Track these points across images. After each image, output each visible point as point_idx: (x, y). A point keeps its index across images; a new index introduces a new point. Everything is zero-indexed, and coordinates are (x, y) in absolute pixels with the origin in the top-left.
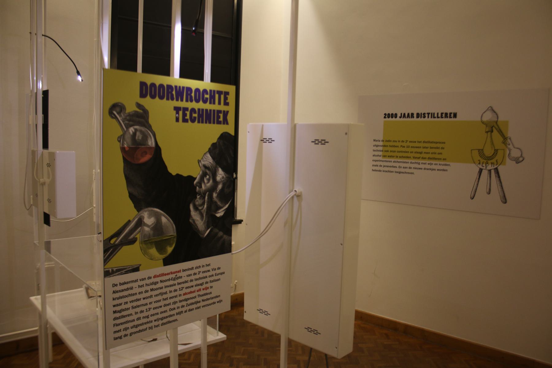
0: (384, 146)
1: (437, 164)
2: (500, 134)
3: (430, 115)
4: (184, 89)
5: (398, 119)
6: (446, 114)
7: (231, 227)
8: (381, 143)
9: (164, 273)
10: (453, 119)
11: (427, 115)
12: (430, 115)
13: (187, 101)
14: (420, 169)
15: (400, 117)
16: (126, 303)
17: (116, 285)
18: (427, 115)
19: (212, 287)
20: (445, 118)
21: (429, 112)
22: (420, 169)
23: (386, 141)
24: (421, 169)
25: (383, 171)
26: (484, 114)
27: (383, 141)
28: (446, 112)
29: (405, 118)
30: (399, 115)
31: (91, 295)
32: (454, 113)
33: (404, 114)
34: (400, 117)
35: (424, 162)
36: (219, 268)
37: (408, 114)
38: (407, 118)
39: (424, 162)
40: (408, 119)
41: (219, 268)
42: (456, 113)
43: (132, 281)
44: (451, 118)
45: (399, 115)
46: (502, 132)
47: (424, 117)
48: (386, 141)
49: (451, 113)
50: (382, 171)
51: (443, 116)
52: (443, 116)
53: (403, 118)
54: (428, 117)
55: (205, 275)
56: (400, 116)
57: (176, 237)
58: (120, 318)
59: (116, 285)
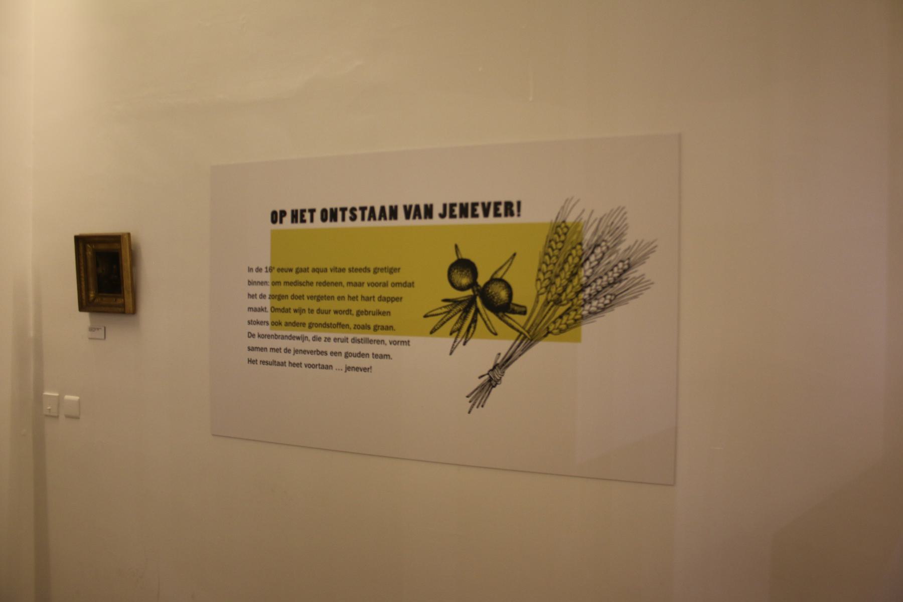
0: (275, 283)
2: (438, 324)
5: (436, 220)
6: (509, 205)
8: (266, 277)
9: (368, 339)
10: (503, 220)
11: (359, 213)
15: (442, 216)
18: (359, 213)
20: (506, 215)
21: (363, 205)
23: (280, 270)
25: (259, 336)
27: (271, 269)
28: (508, 199)
29: (375, 219)
30: (437, 210)
32: (461, 205)
33: (372, 209)
34: (442, 216)
35: (342, 335)
37: (383, 209)
38: (380, 219)
39: (342, 335)
40: (383, 223)
42: (431, 206)
44: (455, 217)
45: (437, 210)
46: (442, 325)
47: (353, 218)
48: (280, 270)
50: (257, 336)
51: (476, 213)
52: (476, 213)
53: (414, 218)
54: (343, 219)
56: (441, 211)
57: (468, 301)
58: (363, 341)
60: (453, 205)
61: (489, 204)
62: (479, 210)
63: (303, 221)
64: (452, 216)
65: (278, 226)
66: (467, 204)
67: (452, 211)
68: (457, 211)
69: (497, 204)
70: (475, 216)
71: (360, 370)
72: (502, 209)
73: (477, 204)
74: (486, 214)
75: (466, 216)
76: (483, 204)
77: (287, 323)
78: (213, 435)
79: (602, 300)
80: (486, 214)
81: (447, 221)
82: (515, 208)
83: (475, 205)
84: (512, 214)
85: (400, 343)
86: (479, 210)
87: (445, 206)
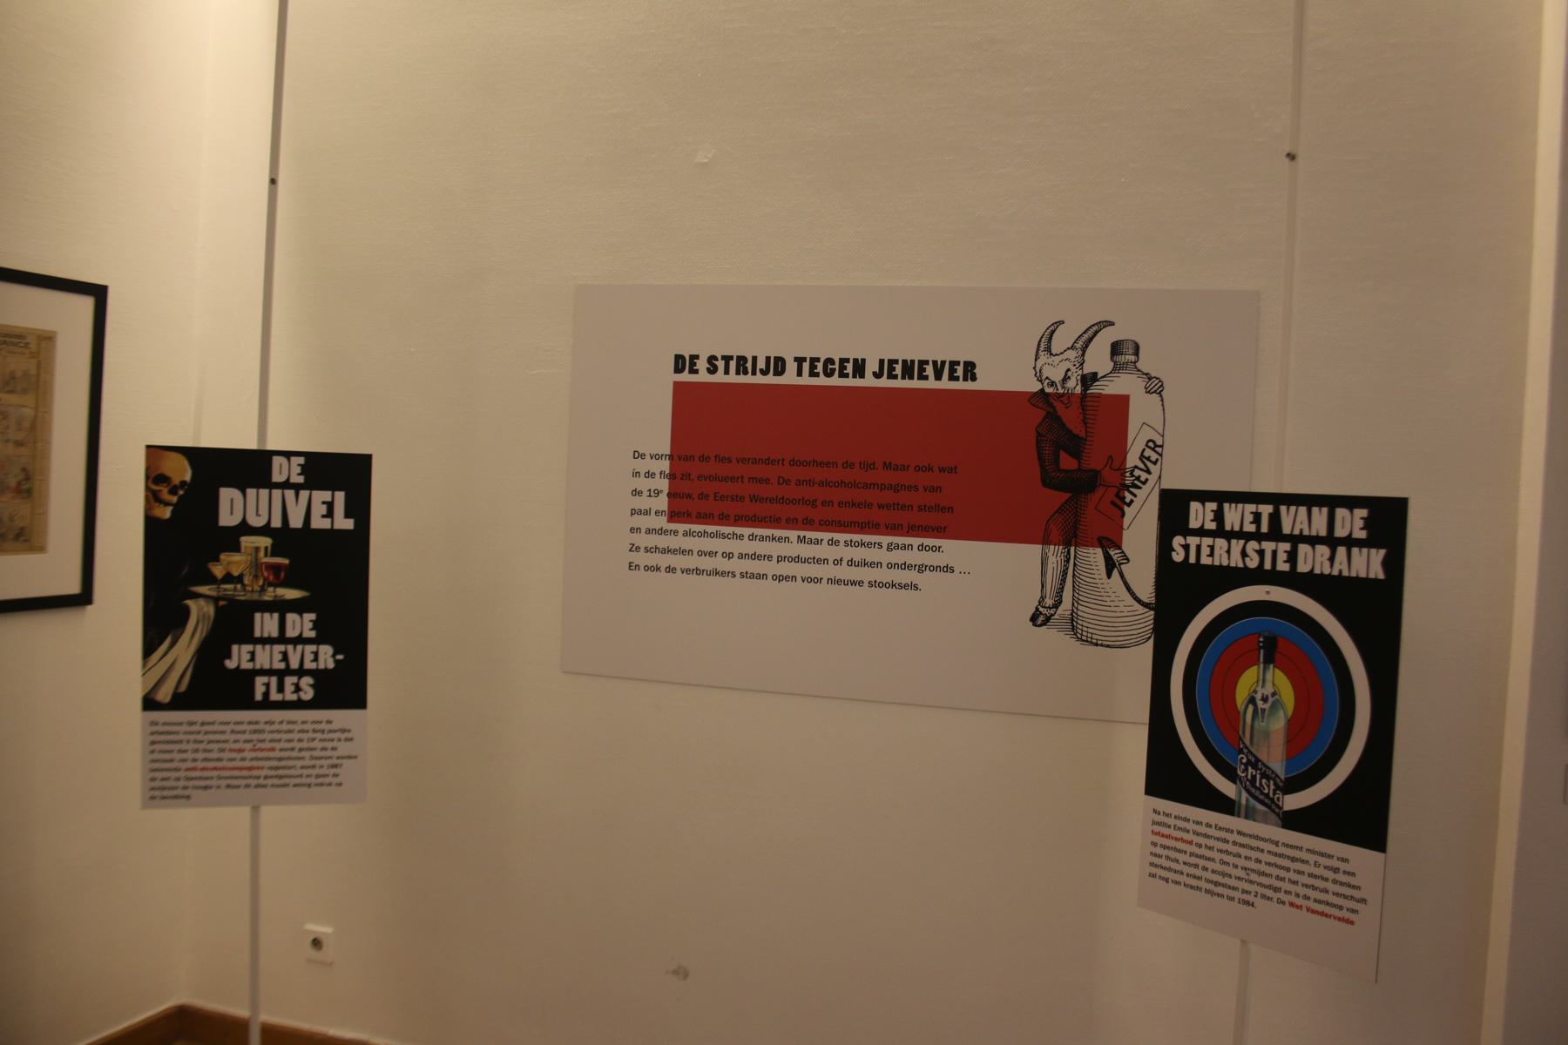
1: (1250, 858)
3: (733, 364)
4: (752, 371)
6: (742, 360)
7: (1301, 573)
11: (721, 364)
12: (733, 364)
13: (738, 373)
14: (854, 583)
15: (877, 375)
16: (729, 556)
17: (642, 456)
18: (721, 364)
19: (675, 972)
22: (854, 583)
24: (860, 583)
26: (1058, 353)
30: (872, 367)
31: (87, 304)
34: (877, 375)
36: (1153, 876)
41: (1153, 876)
43: (855, 523)
49: (843, 361)
55: (1193, 860)
59: (642, 456)
60: (892, 362)
61: (943, 363)
62: (929, 370)
63: (694, 371)
64: (892, 376)
65: (685, 377)
66: (913, 362)
67: (891, 369)
68: (898, 369)
69: (954, 364)
70: (923, 377)
71: (931, 530)
72: (960, 371)
73: (927, 362)
74: (938, 377)
75: (911, 378)
76: (935, 363)
77: (700, 514)
78: (565, 672)
79: (205, 609)
80: (938, 377)
81: (884, 382)
82: (749, 365)
83: (923, 363)
84: (746, 373)
85: (853, 525)
86: (929, 370)
87: (882, 362)
